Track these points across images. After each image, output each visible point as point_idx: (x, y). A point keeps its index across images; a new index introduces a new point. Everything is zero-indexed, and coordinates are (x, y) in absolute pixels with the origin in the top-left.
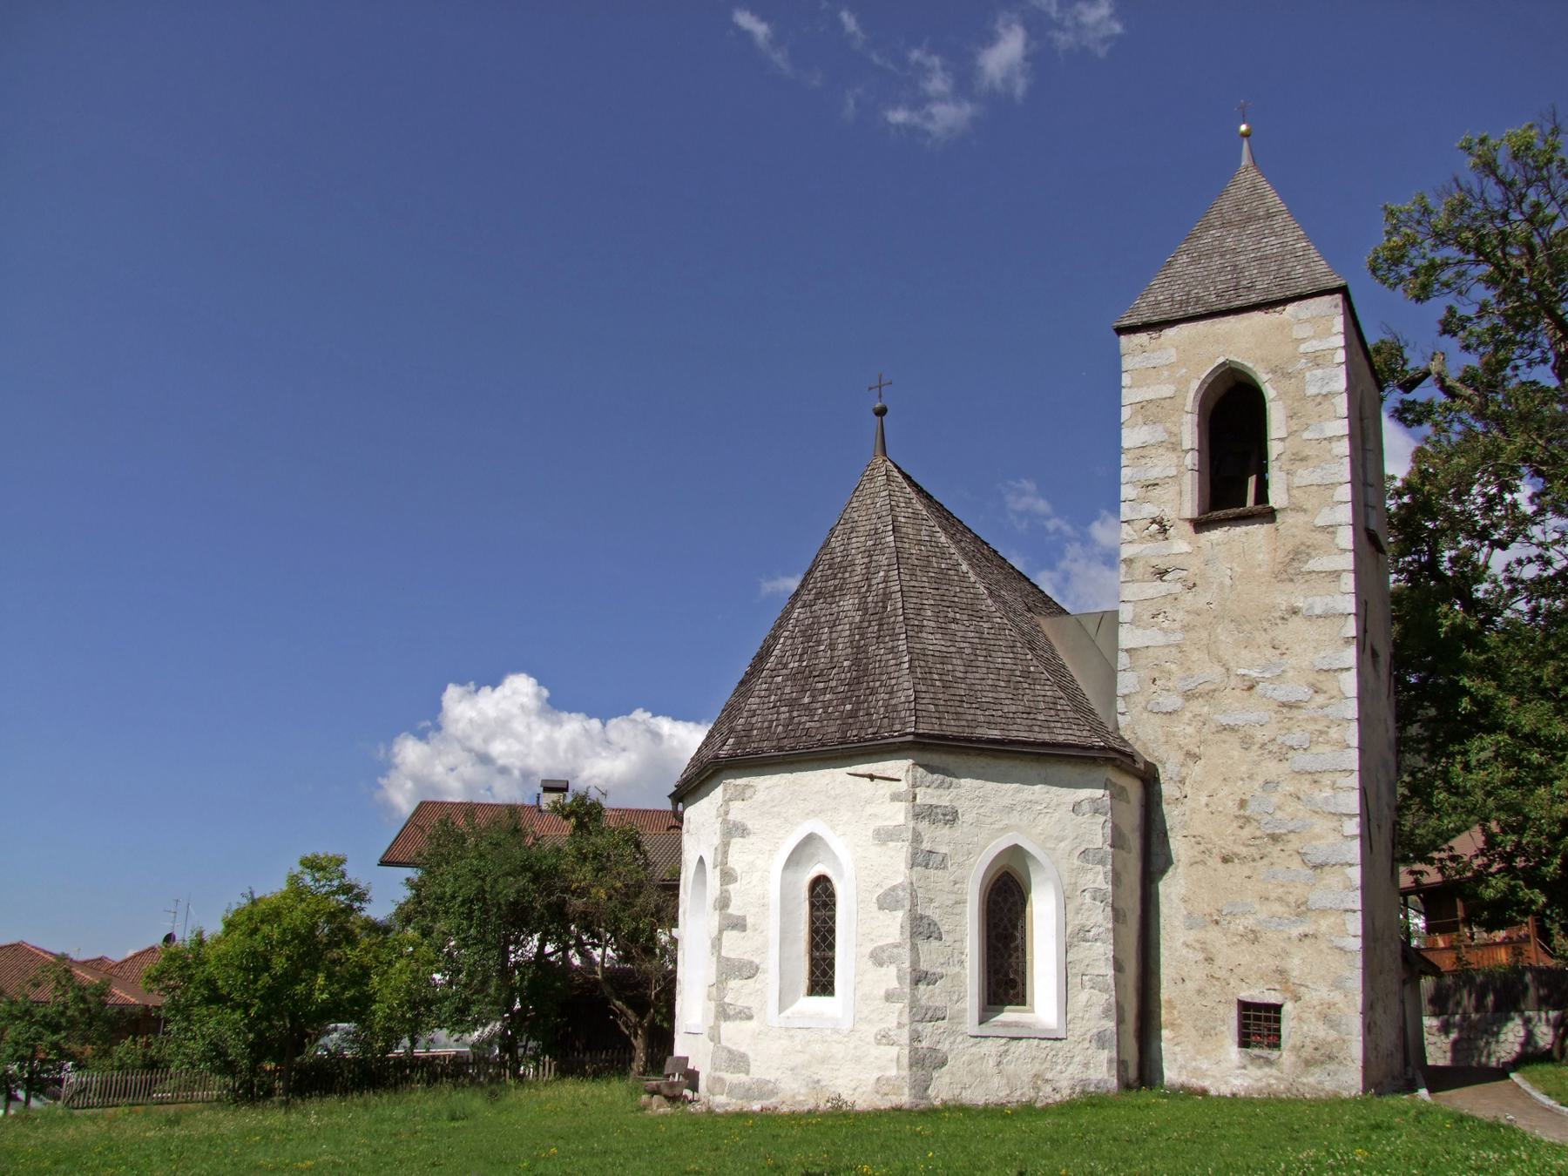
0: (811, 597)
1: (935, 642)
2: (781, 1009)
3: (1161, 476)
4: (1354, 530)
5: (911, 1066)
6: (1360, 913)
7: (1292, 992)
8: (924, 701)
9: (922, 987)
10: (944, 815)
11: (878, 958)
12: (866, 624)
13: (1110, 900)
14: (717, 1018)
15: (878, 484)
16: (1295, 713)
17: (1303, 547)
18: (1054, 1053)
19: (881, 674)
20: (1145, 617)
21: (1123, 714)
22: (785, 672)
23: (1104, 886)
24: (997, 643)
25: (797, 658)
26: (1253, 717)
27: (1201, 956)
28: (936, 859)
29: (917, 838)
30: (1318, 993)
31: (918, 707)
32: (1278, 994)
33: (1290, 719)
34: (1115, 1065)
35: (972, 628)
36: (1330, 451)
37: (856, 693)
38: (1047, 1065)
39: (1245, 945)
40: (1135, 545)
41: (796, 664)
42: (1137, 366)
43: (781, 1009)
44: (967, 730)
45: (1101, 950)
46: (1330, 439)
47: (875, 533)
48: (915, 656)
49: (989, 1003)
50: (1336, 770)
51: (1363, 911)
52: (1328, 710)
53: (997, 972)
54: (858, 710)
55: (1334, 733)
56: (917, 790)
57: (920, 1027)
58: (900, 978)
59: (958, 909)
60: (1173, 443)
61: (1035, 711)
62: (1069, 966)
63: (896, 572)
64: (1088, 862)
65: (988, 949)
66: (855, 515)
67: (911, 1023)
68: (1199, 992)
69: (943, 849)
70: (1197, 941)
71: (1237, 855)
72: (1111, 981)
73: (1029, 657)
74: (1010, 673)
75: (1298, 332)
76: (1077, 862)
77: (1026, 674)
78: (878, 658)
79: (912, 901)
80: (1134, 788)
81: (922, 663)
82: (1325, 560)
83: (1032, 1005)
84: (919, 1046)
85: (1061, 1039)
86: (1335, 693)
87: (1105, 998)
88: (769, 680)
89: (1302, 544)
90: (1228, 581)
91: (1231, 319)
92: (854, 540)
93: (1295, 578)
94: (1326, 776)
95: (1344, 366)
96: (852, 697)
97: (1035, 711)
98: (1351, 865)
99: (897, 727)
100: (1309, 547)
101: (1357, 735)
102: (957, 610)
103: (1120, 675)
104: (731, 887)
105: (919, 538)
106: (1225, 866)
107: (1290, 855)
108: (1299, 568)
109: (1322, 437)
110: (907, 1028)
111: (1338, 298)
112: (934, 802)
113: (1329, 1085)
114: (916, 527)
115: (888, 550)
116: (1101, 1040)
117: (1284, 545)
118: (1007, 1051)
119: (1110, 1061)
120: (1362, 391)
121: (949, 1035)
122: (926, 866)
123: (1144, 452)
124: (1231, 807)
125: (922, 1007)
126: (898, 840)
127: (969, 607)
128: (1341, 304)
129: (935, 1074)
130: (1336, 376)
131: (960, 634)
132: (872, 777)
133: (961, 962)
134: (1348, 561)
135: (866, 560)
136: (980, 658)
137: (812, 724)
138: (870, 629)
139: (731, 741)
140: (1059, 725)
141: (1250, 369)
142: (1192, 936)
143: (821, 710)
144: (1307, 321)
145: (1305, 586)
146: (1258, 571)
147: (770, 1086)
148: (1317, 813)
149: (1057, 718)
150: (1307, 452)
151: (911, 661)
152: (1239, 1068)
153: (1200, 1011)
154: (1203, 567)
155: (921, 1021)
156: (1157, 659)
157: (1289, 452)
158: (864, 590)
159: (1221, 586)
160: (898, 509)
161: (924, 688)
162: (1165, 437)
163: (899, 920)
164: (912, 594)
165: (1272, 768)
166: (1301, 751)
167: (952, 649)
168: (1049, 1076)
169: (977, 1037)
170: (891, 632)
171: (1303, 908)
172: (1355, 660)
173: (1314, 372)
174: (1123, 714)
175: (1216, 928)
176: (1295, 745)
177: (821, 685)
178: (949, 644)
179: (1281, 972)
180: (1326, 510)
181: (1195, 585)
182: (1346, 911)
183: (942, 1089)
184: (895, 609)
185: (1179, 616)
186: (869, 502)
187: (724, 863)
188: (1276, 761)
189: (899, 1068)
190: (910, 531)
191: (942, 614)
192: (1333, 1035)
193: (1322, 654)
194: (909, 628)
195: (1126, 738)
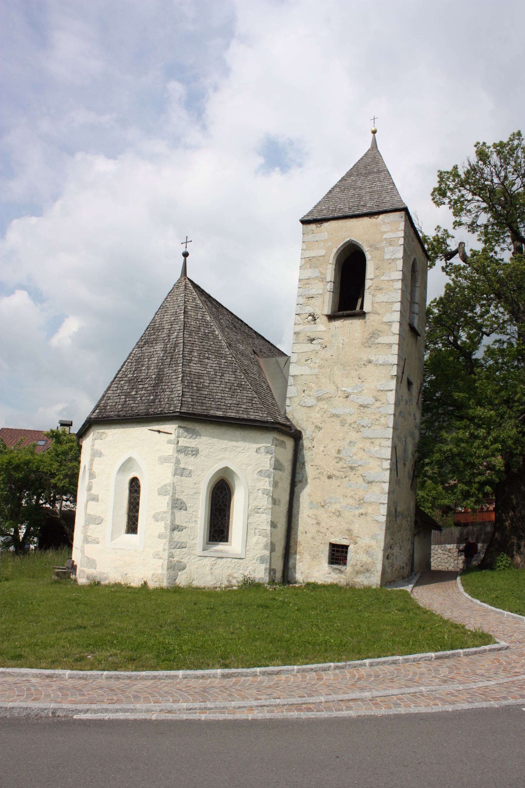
0: (142, 343)
1: (196, 368)
2: (112, 540)
3: (315, 293)
4: (400, 324)
5: (168, 569)
6: (386, 505)
7: (353, 540)
8: (186, 396)
9: (176, 532)
10: (192, 451)
11: (156, 518)
12: (165, 358)
13: (271, 495)
14: (83, 542)
15: (180, 290)
16: (366, 409)
17: (376, 332)
18: (238, 565)
19: (168, 382)
20: (302, 361)
21: (288, 406)
22: (125, 379)
23: (269, 488)
24: (228, 370)
25: (132, 372)
26: (347, 411)
27: (315, 522)
28: (186, 472)
29: (178, 462)
30: (365, 541)
31: (183, 399)
32: (347, 541)
33: (364, 412)
34: (268, 571)
35: (216, 362)
36: (393, 286)
37: (156, 391)
38: (235, 570)
39: (335, 517)
40: (301, 326)
41: (131, 375)
42: (309, 240)
43: (112, 540)
44: (206, 411)
45: (265, 518)
46: (393, 281)
47: (176, 314)
48: (186, 375)
49: (210, 540)
50: (382, 438)
51: (388, 504)
52: (381, 409)
53: (215, 526)
54: (155, 399)
55: (383, 420)
56: (180, 439)
57: (173, 551)
58: (165, 528)
59: (196, 496)
60: (322, 278)
61: (241, 403)
62: (249, 525)
63: (182, 333)
64: (261, 476)
65: (211, 515)
66: (168, 304)
67: (169, 549)
68: (313, 538)
69: (190, 468)
70: (314, 515)
71: (334, 475)
72: (269, 533)
73: (242, 377)
74: (231, 384)
75: (384, 228)
76: (256, 476)
77: (240, 385)
78: (168, 374)
79: (173, 492)
80: (290, 443)
81: (188, 378)
82: (385, 338)
83: (231, 542)
84: (173, 560)
85: (242, 559)
86: (385, 401)
87: (264, 540)
88: (118, 382)
89: (376, 330)
90: (341, 346)
91: (354, 221)
92: (166, 317)
93: (371, 346)
94: (377, 440)
95: (402, 246)
96: (154, 393)
97: (241, 403)
98: (385, 482)
99: (172, 408)
100: (379, 331)
101: (392, 422)
102: (210, 353)
103: (289, 387)
104: (93, 481)
105: (196, 317)
106: (329, 480)
107: (358, 477)
108: (374, 341)
109: (390, 279)
110: (167, 551)
111: (403, 213)
112: (187, 445)
113: (366, 583)
114: (195, 312)
115: (180, 322)
116: (262, 560)
117: (368, 330)
118: (216, 563)
119: (266, 569)
120: (415, 259)
121: (188, 555)
122: (182, 475)
123: (308, 282)
124: (334, 453)
125: (175, 542)
126: (169, 462)
127: (216, 352)
128: (404, 216)
129: (180, 573)
130: (399, 250)
131: (210, 365)
132: (159, 432)
133: (196, 521)
134: (395, 339)
135: (170, 327)
136: (218, 377)
137: (135, 405)
138: (167, 360)
139: (97, 411)
140: (252, 411)
141: (360, 244)
142: (312, 512)
143: (139, 399)
144: (388, 223)
145: (376, 350)
146: (355, 341)
147: (105, 575)
148: (372, 457)
149: (252, 407)
150: (382, 286)
151: (183, 376)
152: (327, 574)
153: (312, 547)
154: (330, 338)
155: (174, 548)
156: (306, 381)
157: (374, 285)
158: (166, 341)
159: (338, 347)
160: (188, 303)
161: (187, 390)
162: (319, 275)
163: (167, 500)
164: (189, 344)
165: (353, 435)
166: (367, 428)
167: (205, 372)
168: (235, 575)
169: (200, 556)
170: (175, 362)
171: (362, 501)
172: (395, 386)
173: (389, 248)
174: (288, 406)
175: (322, 509)
176: (364, 424)
177: (141, 386)
178: (203, 369)
179: (349, 530)
180: (388, 314)
181: (326, 346)
182: (381, 503)
183: (182, 580)
184: (179, 351)
185: (318, 361)
186: (175, 298)
187: (91, 469)
188: (355, 432)
189: (162, 570)
190: (193, 314)
191: (202, 355)
192: (370, 560)
193: (381, 383)
194: (185, 361)
195: (289, 418)
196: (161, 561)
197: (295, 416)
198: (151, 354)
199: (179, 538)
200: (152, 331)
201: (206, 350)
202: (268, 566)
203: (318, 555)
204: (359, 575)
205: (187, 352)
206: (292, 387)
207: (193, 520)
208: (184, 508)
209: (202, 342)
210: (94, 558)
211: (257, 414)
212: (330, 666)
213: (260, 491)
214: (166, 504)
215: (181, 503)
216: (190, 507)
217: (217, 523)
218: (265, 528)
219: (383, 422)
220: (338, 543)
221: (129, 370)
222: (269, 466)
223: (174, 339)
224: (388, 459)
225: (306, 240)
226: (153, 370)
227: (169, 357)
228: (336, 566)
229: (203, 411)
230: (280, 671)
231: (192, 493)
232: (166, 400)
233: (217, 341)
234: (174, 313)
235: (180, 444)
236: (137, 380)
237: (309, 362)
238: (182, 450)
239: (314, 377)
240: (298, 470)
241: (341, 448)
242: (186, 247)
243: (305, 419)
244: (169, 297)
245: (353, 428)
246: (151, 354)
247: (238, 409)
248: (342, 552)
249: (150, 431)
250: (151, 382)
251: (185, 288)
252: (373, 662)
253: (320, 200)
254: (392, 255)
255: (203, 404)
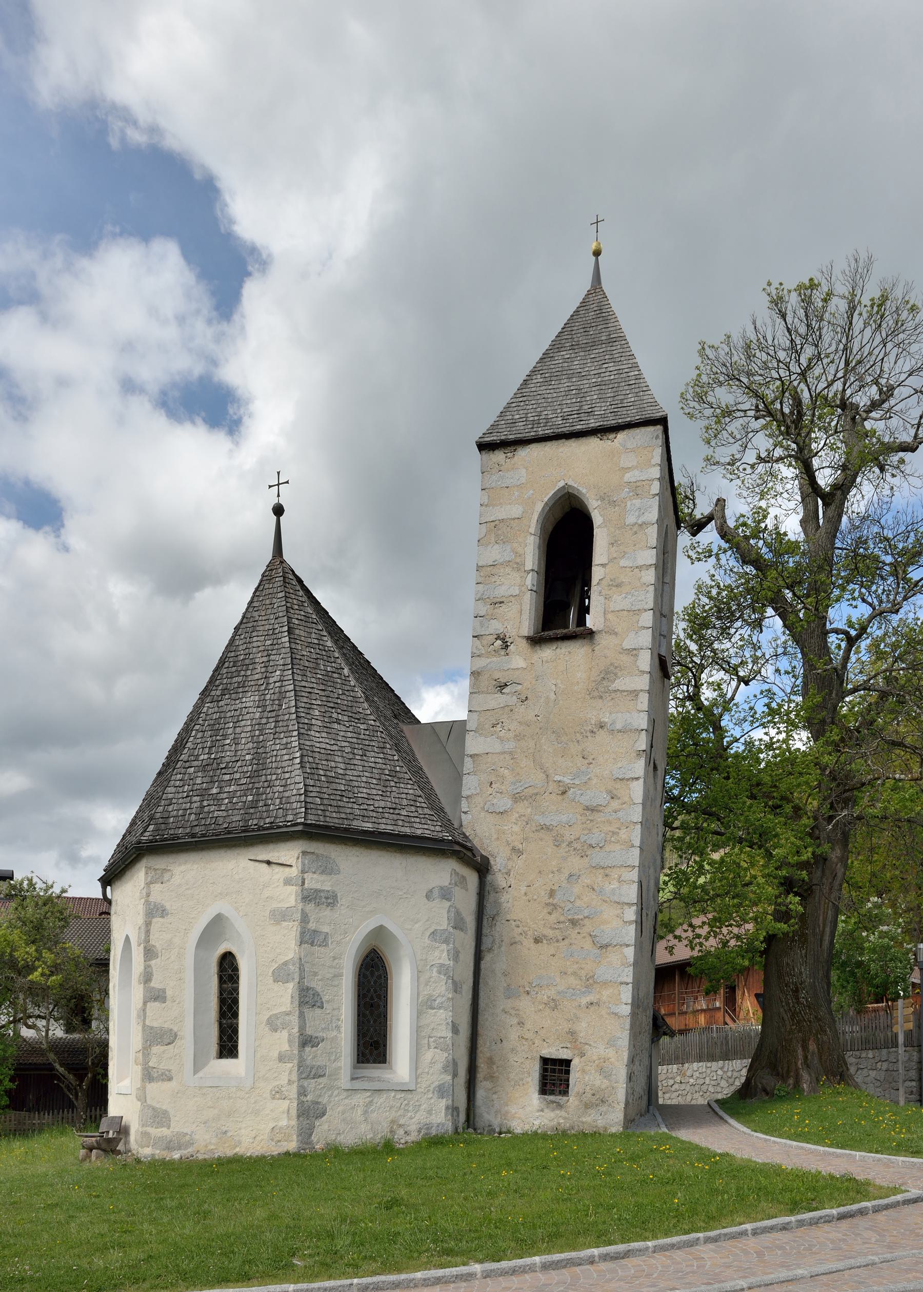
1: (321, 740)
3: (507, 594)
5: (299, 1117)
8: (312, 794)
9: (308, 1049)
10: (327, 898)
12: (264, 721)
14: (143, 1080)
17: (612, 668)
18: (406, 1102)
21: (465, 813)
22: (195, 763)
23: (447, 962)
25: (207, 750)
26: (564, 818)
29: (305, 919)
30: (598, 1050)
33: (591, 821)
35: (351, 729)
36: (640, 579)
37: (256, 785)
38: (401, 1112)
41: (206, 757)
42: (493, 485)
44: (346, 822)
45: (443, 1016)
46: (640, 568)
49: (358, 1062)
50: (622, 866)
52: (620, 814)
55: (623, 834)
56: (306, 875)
57: (306, 1083)
58: (289, 1041)
60: (517, 563)
61: (399, 807)
63: (290, 672)
66: (256, 614)
67: (299, 1080)
69: (325, 929)
71: (545, 936)
72: (449, 1042)
73: (396, 758)
76: (427, 941)
77: (393, 774)
78: (275, 753)
79: (300, 975)
81: (311, 760)
84: (305, 1099)
86: (626, 799)
88: (183, 771)
89: (612, 664)
90: (553, 696)
92: (255, 639)
96: (252, 789)
98: (628, 946)
99: (290, 818)
100: (616, 667)
102: (339, 711)
103: (465, 777)
104: (153, 963)
107: (584, 937)
108: (608, 687)
109: (635, 564)
110: (296, 1084)
113: (601, 1123)
114: (307, 629)
115: (283, 650)
116: (441, 1091)
118: (371, 1102)
119: (447, 1108)
121: (329, 1089)
122: (312, 944)
123: (494, 571)
125: (307, 1067)
127: (349, 709)
129: (317, 1123)
132: (269, 863)
133: (338, 1028)
138: (268, 726)
140: (418, 820)
144: (633, 450)
145: (611, 704)
147: (187, 1138)
149: (416, 814)
151: (302, 756)
152: (538, 1111)
154: (534, 682)
155: (307, 1078)
156: (494, 764)
158: (263, 687)
163: (290, 991)
164: (303, 694)
165: (576, 863)
166: (598, 849)
170: (285, 729)
173: (634, 501)
174: (465, 813)
176: (593, 842)
177: (227, 777)
178: (333, 742)
179: (572, 1033)
186: (268, 602)
187: (147, 940)
188: (578, 858)
189: (289, 1119)
190: (302, 633)
193: (619, 765)
194: (301, 726)
196: (287, 1102)
197: (478, 831)
198: (238, 713)
199: (314, 1057)
200: (234, 669)
201: (332, 705)
202: (450, 1102)
203: (522, 1079)
204: (592, 1111)
205: (302, 710)
206: (472, 777)
207: (334, 1025)
208: (319, 1004)
209: (324, 690)
210: (164, 1108)
211: (426, 827)
212: (698, 1239)
213: (435, 969)
214: (290, 998)
215: (314, 995)
216: (328, 1002)
217: (368, 1030)
218: (444, 1034)
219: (624, 836)
220: (554, 1057)
221: (200, 746)
222: (446, 922)
223: (277, 684)
224: (633, 904)
225: (487, 486)
226: (246, 747)
227: (271, 720)
228: (552, 1098)
229: (340, 821)
230: (629, 1251)
231: (330, 976)
232: (278, 801)
233: (349, 688)
234: (271, 632)
235: (306, 885)
236: (218, 764)
237: (499, 728)
238: (310, 897)
239: (507, 757)
240: (485, 931)
241: (556, 887)
242: (278, 496)
243: (495, 836)
244: (256, 599)
245: (574, 849)
246: (238, 713)
247: (395, 817)
248: (560, 1071)
249: (252, 863)
250: (245, 769)
251: (284, 582)
252: (757, 1229)
253: (508, 400)
254: (639, 516)
255: (342, 810)
